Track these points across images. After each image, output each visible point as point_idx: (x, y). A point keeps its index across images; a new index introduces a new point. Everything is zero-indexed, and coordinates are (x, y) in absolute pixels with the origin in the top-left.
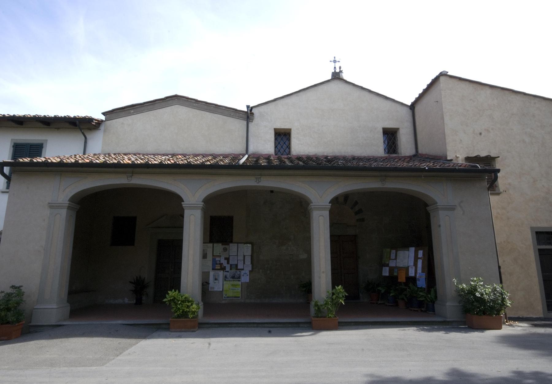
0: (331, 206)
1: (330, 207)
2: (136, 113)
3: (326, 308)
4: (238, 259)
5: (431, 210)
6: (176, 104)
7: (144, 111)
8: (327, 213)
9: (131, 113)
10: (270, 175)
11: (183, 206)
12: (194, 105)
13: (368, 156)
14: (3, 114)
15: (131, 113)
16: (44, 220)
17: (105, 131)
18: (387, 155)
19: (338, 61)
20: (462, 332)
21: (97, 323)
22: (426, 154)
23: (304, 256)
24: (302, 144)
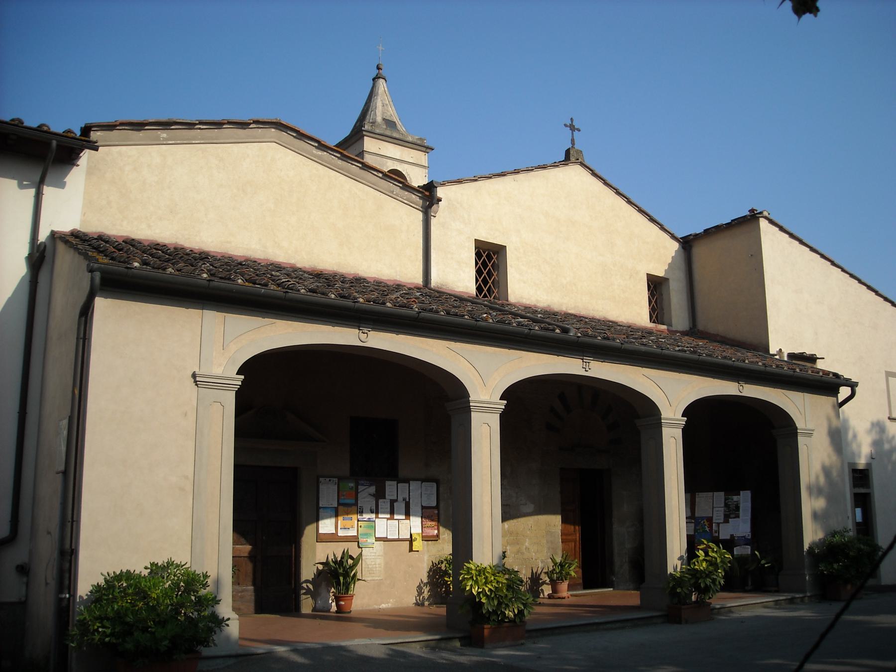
0: (686, 422)
1: (503, 407)
2: (173, 142)
3: (183, 612)
4: (714, 506)
5: (465, 407)
6: (272, 140)
7: (194, 142)
8: (229, 399)
9: (160, 140)
10: (272, 313)
11: (471, 404)
12: (314, 152)
13: (627, 323)
14: (115, 131)
15: (160, 140)
16: (186, 415)
17: (90, 172)
18: (652, 325)
19: (570, 120)
20: (320, 646)
21: (781, 598)
22: (718, 335)
23: (703, 499)
24: (524, 282)
